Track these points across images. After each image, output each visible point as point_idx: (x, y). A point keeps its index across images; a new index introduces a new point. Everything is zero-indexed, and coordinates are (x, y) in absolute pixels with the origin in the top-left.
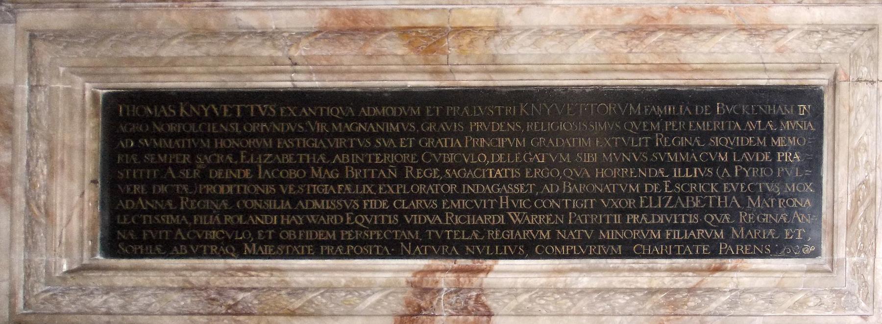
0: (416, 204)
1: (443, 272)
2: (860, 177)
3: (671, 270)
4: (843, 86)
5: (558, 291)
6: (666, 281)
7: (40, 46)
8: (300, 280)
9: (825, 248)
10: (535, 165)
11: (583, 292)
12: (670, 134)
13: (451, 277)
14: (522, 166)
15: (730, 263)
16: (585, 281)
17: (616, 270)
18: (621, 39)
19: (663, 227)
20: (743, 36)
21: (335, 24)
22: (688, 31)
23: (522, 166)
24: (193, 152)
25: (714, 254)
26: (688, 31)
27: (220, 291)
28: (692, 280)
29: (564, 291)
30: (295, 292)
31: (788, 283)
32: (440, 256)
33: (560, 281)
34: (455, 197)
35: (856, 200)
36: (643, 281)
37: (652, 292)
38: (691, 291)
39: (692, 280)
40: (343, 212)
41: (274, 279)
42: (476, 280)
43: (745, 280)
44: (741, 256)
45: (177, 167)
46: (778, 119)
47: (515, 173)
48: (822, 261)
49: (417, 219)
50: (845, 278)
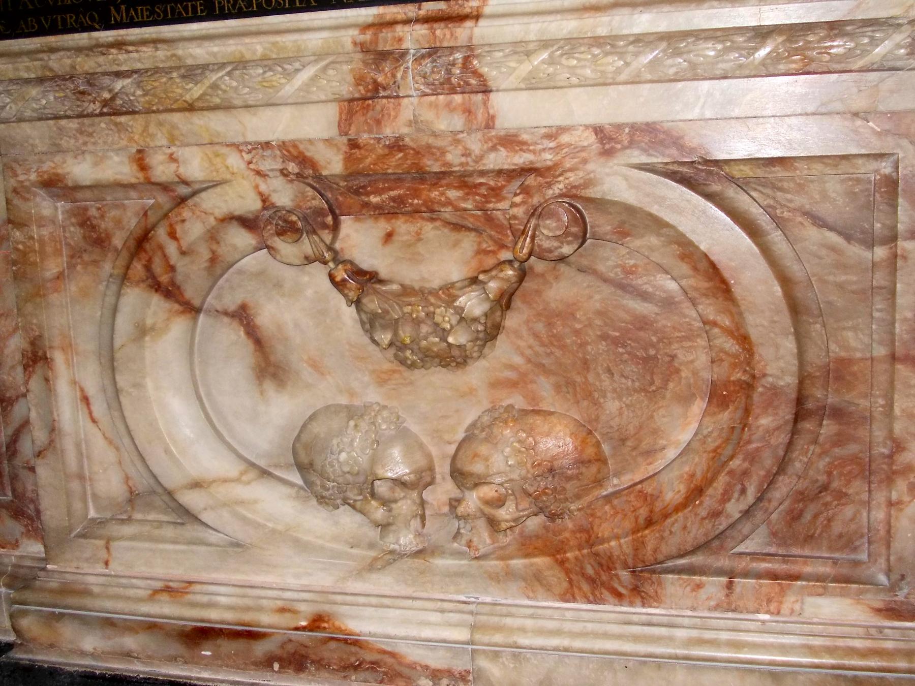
5: (597, 41)
8: (198, 53)
11: (641, 41)
13: (421, 30)
30: (193, 72)
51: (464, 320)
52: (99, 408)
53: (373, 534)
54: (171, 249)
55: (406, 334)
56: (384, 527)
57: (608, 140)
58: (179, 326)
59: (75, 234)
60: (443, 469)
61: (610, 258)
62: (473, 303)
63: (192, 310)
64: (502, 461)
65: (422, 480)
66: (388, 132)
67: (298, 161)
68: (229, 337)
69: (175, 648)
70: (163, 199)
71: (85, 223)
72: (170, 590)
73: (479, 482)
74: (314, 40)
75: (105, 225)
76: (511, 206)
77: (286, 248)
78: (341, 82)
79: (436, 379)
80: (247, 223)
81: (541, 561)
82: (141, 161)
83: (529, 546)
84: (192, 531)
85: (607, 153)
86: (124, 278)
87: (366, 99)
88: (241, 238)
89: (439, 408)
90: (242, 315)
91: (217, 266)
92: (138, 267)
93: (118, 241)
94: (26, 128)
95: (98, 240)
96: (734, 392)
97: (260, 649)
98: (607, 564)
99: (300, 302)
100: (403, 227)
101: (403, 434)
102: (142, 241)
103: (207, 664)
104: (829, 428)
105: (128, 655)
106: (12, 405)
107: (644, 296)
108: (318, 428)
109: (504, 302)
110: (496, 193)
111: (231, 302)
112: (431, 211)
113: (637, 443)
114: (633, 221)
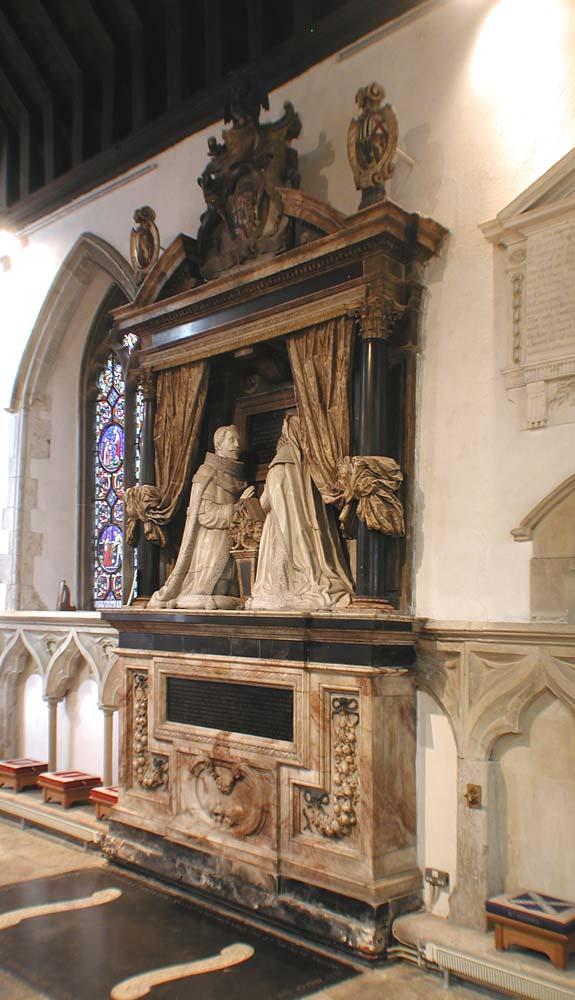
8: (198, 732)
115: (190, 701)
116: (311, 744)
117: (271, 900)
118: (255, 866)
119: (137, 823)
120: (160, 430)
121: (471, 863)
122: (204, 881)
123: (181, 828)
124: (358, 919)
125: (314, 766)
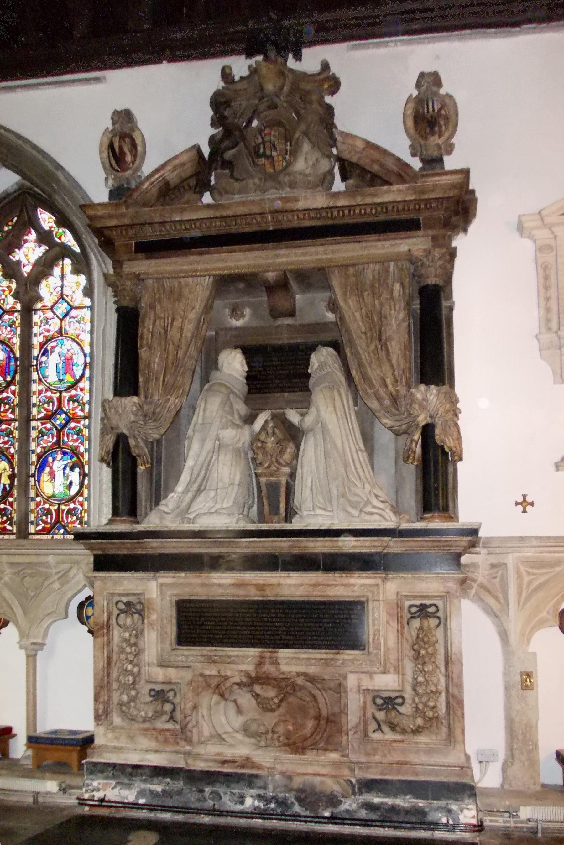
0: (258, 633)
1: (267, 652)
2: (376, 628)
3: (325, 653)
4: (370, 602)
5: (296, 658)
6: (324, 656)
7: (164, 588)
8: (231, 654)
9: (366, 648)
10: (288, 622)
11: (303, 659)
12: (323, 614)
13: (269, 654)
14: (284, 622)
15: (341, 651)
16: (303, 656)
17: (311, 653)
18: (311, 588)
19: (323, 641)
20: (343, 587)
21: (237, 583)
22: (328, 585)
23: (284, 622)
24: (200, 617)
25: (337, 649)
26: (328, 585)
27: (211, 656)
28: (331, 656)
29: (298, 658)
30: (229, 657)
31: (357, 658)
32: (266, 648)
33: (297, 656)
34: (267, 631)
35: (375, 635)
36: (319, 656)
37: (321, 659)
38: (332, 659)
39: (331, 656)
40: (238, 634)
41: (224, 653)
42: (276, 655)
43: (346, 657)
44: (343, 649)
45: (196, 621)
46: (352, 610)
47: (283, 624)
48: (366, 652)
49: (258, 637)
50: (372, 657)
51: (275, 703)
52: (206, 718)
53: (257, 743)
54: (224, 688)
55: (265, 706)
56: (259, 741)
57: (298, 674)
58: (223, 703)
59: (204, 684)
60: (270, 731)
61: (299, 694)
62: (276, 701)
63: (226, 700)
64: (281, 729)
65: (267, 733)
66: (263, 670)
67: (248, 675)
68: (232, 705)
69: (220, 765)
70: (223, 679)
71: (206, 682)
72: (218, 754)
73: (277, 733)
74: (252, 653)
75: (211, 683)
76: (283, 684)
77: (245, 689)
78: (256, 660)
79: (270, 714)
80: (237, 684)
81: (287, 747)
82: (219, 671)
83: (285, 745)
84: (223, 743)
85: (298, 676)
86: (214, 693)
87: (260, 664)
88: (236, 687)
89: (270, 719)
90: (235, 701)
91: (231, 692)
92: (217, 691)
93: (213, 686)
94: (197, 664)
95: (209, 686)
96: (318, 718)
97: (236, 764)
98: (298, 748)
99: (246, 699)
100: (264, 686)
101: (264, 725)
102: (218, 686)
103: (226, 768)
104: (332, 724)
105: (210, 767)
106: (442, 622)
107: (304, 701)
108: (248, 722)
109: (281, 701)
110: (280, 682)
111: (233, 698)
112: (269, 684)
113: (303, 726)
114: (302, 688)
115: (198, 624)
116: (387, 650)
117: (348, 805)
118: (323, 775)
119: (134, 759)
120: (145, 342)
121: (525, 736)
122: (249, 802)
123: (205, 756)
124: (457, 800)
125: (392, 670)
